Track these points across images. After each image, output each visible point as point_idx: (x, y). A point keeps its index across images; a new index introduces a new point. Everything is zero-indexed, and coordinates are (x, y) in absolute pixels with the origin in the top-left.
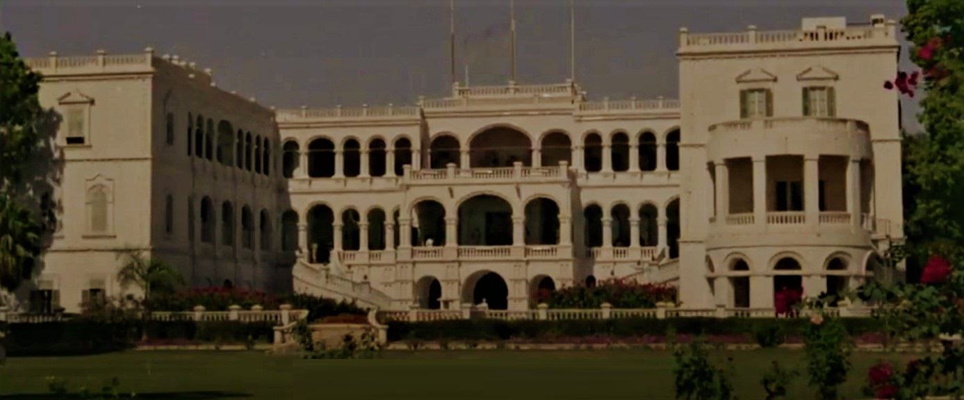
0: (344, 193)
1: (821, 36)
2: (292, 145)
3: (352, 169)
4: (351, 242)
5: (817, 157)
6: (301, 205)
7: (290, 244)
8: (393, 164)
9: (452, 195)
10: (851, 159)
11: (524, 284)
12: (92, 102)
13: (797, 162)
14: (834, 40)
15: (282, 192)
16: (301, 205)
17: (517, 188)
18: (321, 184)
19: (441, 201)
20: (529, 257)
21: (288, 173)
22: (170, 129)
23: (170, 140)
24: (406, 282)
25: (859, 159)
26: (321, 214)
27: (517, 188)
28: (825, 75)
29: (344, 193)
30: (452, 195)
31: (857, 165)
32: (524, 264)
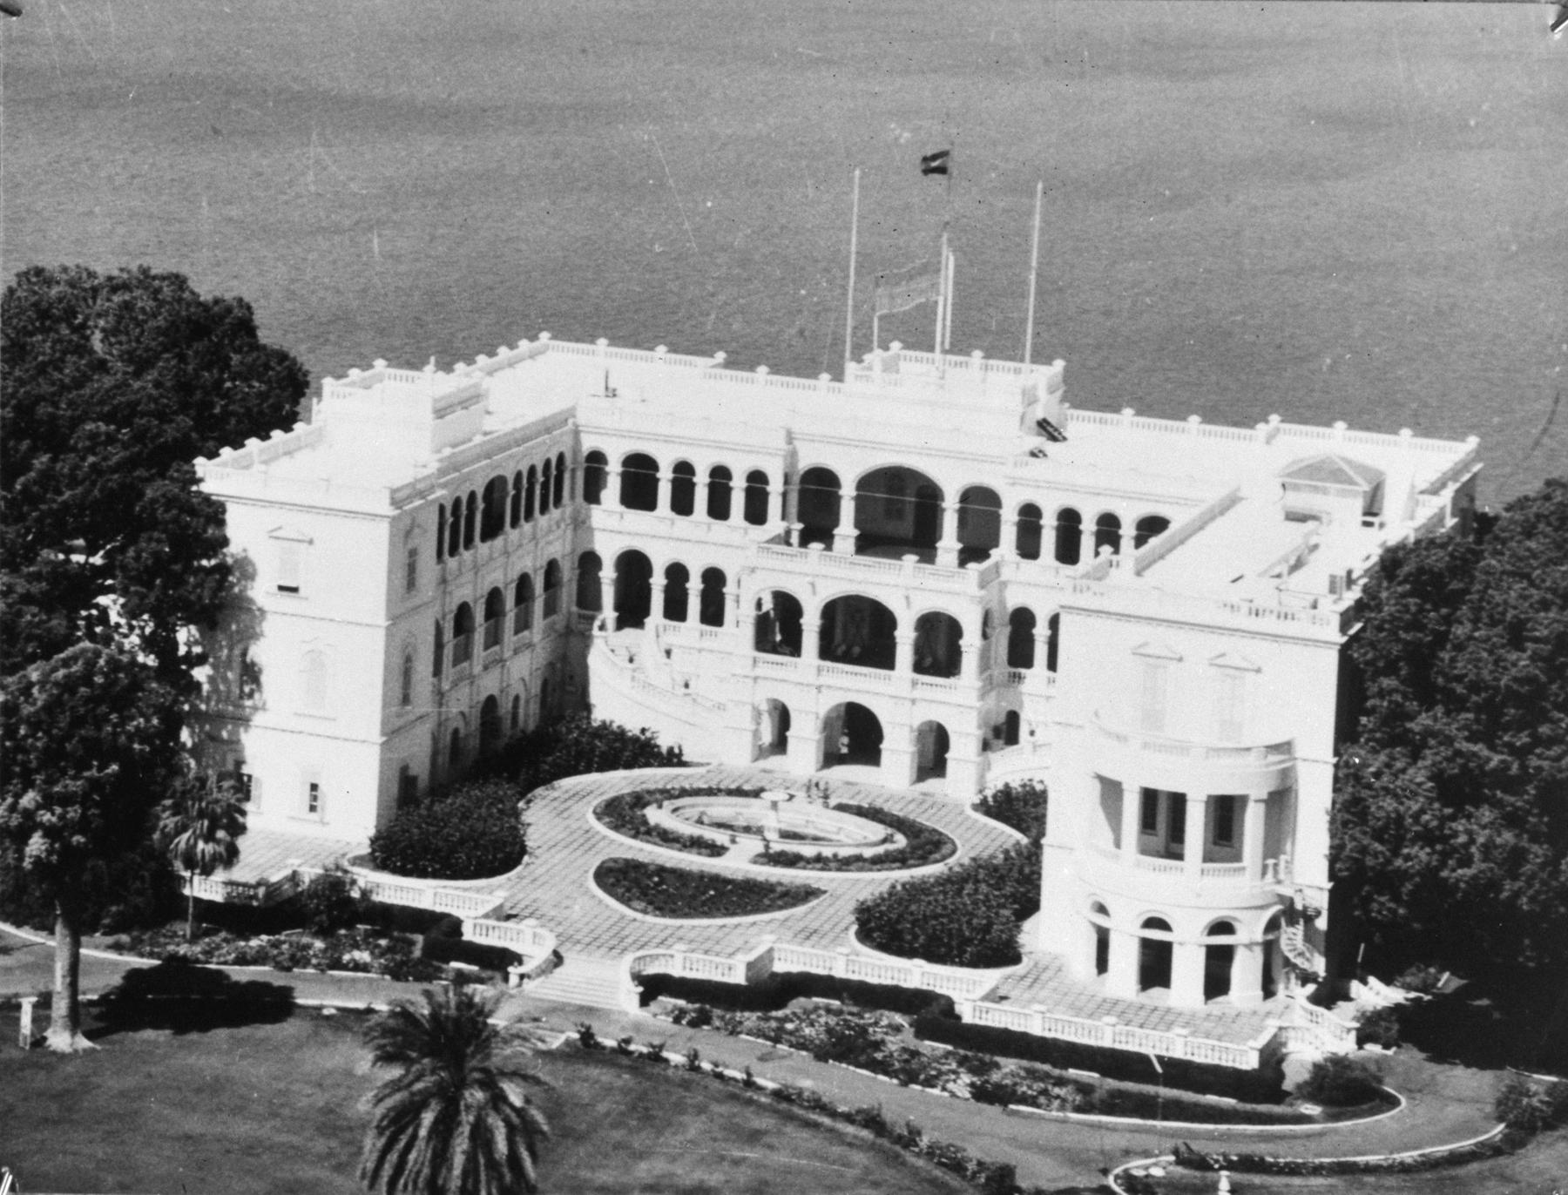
0: (665, 537)
1: (1245, 610)
2: (597, 458)
3: (682, 504)
4: (675, 610)
5: (1205, 798)
6: (609, 550)
7: (588, 599)
8: (642, 858)
9: (814, 593)
10: (1252, 797)
11: (907, 729)
12: (311, 542)
13: (1178, 802)
14: (1260, 619)
15: (580, 524)
16: (609, 550)
17: (905, 588)
18: (637, 519)
19: (797, 596)
20: (917, 694)
21: (592, 496)
22: (412, 569)
23: (411, 584)
24: (744, 704)
25: (1265, 796)
26: (634, 566)
27: (905, 588)
28: (1244, 665)
29: (665, 537)
30: (814, 593)
31: (1262, 807)
32: (908, 704)
